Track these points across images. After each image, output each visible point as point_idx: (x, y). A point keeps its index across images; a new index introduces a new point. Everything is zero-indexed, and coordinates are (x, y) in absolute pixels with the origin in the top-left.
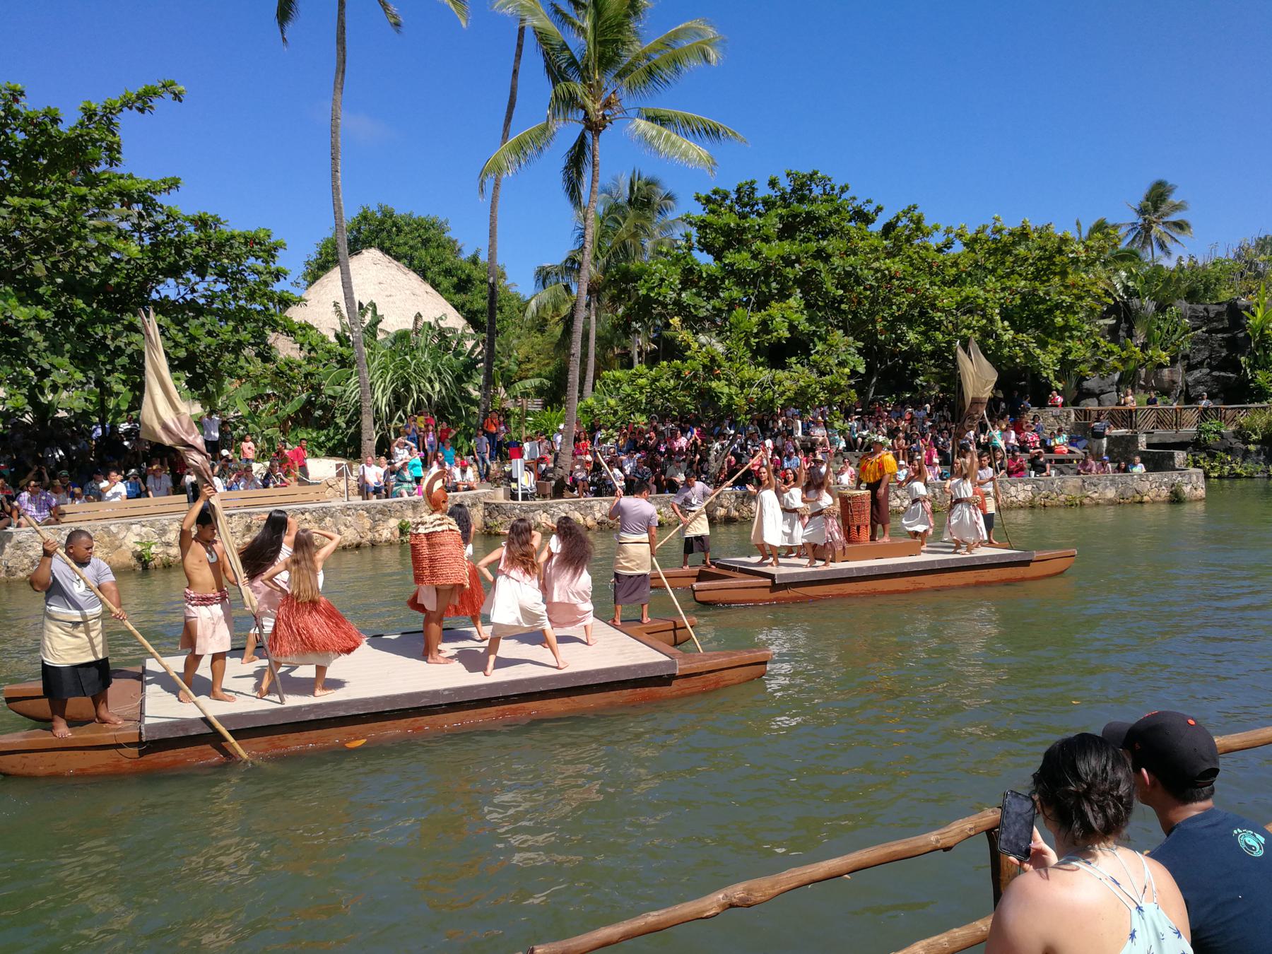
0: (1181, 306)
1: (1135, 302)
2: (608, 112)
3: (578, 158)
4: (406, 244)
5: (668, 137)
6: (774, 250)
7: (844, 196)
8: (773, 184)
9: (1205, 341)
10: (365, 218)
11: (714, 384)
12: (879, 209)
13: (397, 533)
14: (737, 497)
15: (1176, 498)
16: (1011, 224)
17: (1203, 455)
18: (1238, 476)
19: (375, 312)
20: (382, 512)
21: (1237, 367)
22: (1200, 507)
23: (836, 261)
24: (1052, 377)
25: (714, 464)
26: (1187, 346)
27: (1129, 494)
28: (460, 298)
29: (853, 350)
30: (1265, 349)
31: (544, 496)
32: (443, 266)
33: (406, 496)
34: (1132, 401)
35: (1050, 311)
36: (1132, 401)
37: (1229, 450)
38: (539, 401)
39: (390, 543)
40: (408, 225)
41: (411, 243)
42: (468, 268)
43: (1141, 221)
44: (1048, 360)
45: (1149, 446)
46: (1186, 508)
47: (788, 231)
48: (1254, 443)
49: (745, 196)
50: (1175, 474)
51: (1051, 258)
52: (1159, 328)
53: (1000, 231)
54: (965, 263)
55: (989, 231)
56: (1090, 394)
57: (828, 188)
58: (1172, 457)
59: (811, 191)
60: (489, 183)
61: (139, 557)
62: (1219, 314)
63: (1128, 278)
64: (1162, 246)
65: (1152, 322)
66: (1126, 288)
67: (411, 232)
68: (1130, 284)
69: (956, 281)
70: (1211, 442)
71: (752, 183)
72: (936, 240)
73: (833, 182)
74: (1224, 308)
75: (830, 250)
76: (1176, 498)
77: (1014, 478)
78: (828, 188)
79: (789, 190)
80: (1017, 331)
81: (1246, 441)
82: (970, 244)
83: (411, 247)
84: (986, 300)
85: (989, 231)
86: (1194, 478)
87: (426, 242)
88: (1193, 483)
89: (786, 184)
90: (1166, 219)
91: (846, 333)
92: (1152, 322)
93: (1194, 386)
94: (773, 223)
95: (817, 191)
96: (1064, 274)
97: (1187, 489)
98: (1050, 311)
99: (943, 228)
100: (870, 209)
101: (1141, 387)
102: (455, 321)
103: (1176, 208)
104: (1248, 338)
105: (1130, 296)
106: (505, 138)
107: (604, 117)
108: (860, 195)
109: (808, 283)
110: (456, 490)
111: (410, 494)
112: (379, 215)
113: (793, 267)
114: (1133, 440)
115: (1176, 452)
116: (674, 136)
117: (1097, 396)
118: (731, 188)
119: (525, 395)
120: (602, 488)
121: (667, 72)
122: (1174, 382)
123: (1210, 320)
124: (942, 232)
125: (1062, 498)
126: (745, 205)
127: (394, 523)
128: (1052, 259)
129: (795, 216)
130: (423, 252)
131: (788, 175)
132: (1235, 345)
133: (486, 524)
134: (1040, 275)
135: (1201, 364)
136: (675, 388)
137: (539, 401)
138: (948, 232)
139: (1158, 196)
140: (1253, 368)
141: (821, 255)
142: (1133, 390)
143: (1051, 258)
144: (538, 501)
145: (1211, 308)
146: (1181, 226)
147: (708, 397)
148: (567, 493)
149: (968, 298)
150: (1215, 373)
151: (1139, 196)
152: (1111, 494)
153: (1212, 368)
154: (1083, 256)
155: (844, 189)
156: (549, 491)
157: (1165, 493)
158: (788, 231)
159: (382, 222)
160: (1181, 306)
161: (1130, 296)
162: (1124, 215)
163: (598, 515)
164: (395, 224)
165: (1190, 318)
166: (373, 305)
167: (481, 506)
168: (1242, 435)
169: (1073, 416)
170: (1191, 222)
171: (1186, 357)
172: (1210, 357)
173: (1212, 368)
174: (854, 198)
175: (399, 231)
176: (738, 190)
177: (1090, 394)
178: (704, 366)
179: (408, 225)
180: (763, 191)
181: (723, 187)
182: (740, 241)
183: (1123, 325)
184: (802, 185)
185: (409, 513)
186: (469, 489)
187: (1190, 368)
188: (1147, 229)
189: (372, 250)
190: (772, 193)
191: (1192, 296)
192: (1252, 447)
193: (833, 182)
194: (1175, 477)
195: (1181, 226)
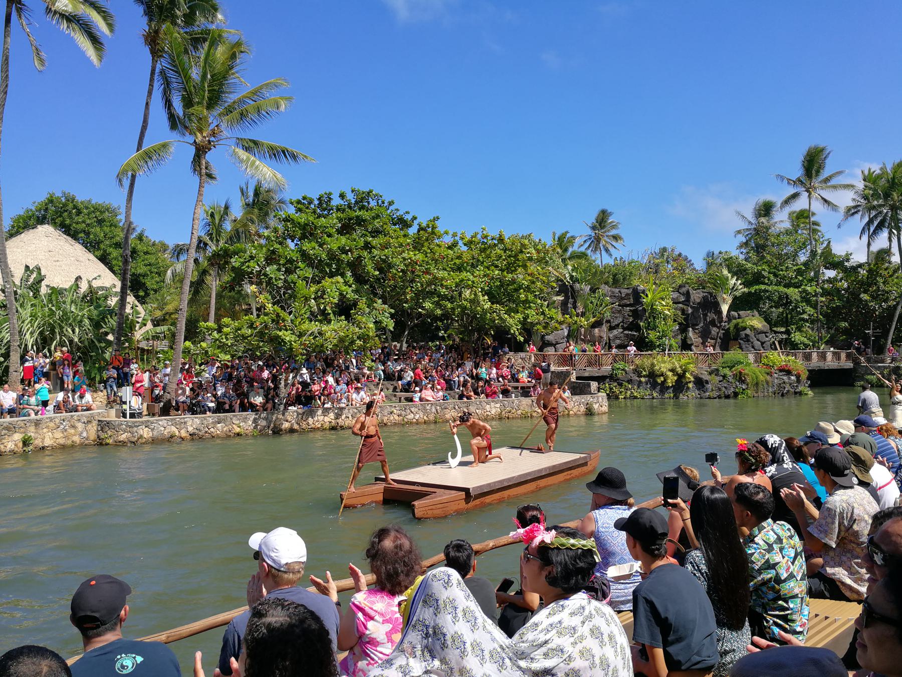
0: (604, 289)
1: (577, 286)
2: (212, 139)
4: (84, 222)
5: (254, 162)
6: (336, 243)
7: (391, 208)
8: (342, 196)
9: (620, 312)
10: (51, 201)
11: (280, 334)
12: (415, 218)
13: (21, 445)
14: (298, 414)
15: (589, 413)
16: (493, 233)
17: (615, 384)
18: (636, 398)
19: (39, 273)
20: (7, 428)
21: (638, 328)
22: (605, 418)
23: (375, 252)
24: (517, 333)
25: (283, 390)
26: (608, 315)
29: (387, 315)
30: (654, 318)
31: (154, 415)
32: (114, 241)
33: (33, 416)
34: (573, 348)
35: (516, 290)
36: (573, 348)
37: (630, 381)
39: (13, 452)
40: (87, 208)
41: (88, 221)
43: (593, 234)
44: (513, 323)
45: (578, 378)
46: (596, 418)
47: (346, 229)
48: (644, 376)
49: (324, 202)
50: (589, 396)
51: (516, 256)
52: (592, 303)
53: (486, 237)
54: (466, 257)
55: (479, 236)
56: (549, 344)
57: (380, 202)
58: (589, 385)
59: (369, 203)
60: (126, 183)
62: (627, 295)
63: (573, 270)
64: (607, 250)
65: (588, 299)
66: (572, 277)
67: (89, 214)
68: (574, 274)
69: (459, 269)
70: (619, 376)
71: (330, 194)
72: (448, 240)
73: (383, 198)
74: (630, 291)
76: (589, 413)
77: (490, 399)
78: (380, 202)
79: (353, 201)
80: (493, 303)
81: (640, 376)
82: (469, 244)
83: (88, 225)
84: (473, 282)
85: (479, 236)
86: (600, 399)
87: (100, 222)
88: (600, 402)
89: (351, 197)
90: (608, 234)
91: (384, 303)
92: (588, 299)
93: (614, 340)
94: (333, 221)
95: (373, 203)
96: (525, 267)
97: (596, 406)
98: (516, 290)
99: (451, 233)
100: (408, 217)
101: (582, 340)
102: (108, 280)
103: (614, 227)
104: (644, 310)
105: (574, 282)
107: (209, 142)
108: (403, 207)
109: (356, 265)
110: (76, 411)
111: (36, 414)
112: (63, 200)
113: (347, 254)
114: (567, 374)
115: (592, 383)
116: (258, 162)
117: (554, 345)
118: (315, 196)
120: (195, 408)
121: (253, 115)
122: (601, 337)
123: (622, 299)
124: (450, 236)
125: (519, 412)
126: (324, 210)
127: (18, 437)
128: (514, 256)
129: (350, 219)
130: (98, 229)
131: (353, 191)
132: (636, 315)
133: (98, 437)
134: (510, 268)
135: (618, 325)
136: (251, 335)
138: (454, 235)
139: (602, 220)
140: (647, 329)
141: (367, 246)
142: (576, 342)
143: (516, 256)
144: (145, 418)
145: (623, 291)
146: (616, 238)
147: (277, 342)
148: (173, 412)
149: (463, 280)
150: (626, 332)
151: (592, 219)
153: (624, 329)
154: (535, 256)
155: (391, 203)
156: (157, 410)
157: (583, 409)
158: (346, 229)
159: (65, 205)
160: (604, 289)
161: (574, 282)
162: (581, 233)
163: (190, 429)
164: (75, 207)
165: (610, 297)
166: (39, 269)
167: (95, 423)
168: (637, 372)
169: (533, 358)
170: (623, 236)
171: (608, 321)
172: (623, 322)
173: (624, 329)
174: (397, 210)
175: (79, 212)
176: (319, 199)
177: (549, 344)
178: (273, 321)
179: (87, 208)
180: (336, 201)
181: (309, 195)
182: (311, 234)
183: (571, 300)
184: (362, 199)
185: (32, 429)
187: (611, 328)
188: (598, 240)
189: (46, 226)
190: (342, 202)
191: (616, 282)
192: (643, 379)
193: (383, 198)
194: (588, 398)
195: (616, 238)
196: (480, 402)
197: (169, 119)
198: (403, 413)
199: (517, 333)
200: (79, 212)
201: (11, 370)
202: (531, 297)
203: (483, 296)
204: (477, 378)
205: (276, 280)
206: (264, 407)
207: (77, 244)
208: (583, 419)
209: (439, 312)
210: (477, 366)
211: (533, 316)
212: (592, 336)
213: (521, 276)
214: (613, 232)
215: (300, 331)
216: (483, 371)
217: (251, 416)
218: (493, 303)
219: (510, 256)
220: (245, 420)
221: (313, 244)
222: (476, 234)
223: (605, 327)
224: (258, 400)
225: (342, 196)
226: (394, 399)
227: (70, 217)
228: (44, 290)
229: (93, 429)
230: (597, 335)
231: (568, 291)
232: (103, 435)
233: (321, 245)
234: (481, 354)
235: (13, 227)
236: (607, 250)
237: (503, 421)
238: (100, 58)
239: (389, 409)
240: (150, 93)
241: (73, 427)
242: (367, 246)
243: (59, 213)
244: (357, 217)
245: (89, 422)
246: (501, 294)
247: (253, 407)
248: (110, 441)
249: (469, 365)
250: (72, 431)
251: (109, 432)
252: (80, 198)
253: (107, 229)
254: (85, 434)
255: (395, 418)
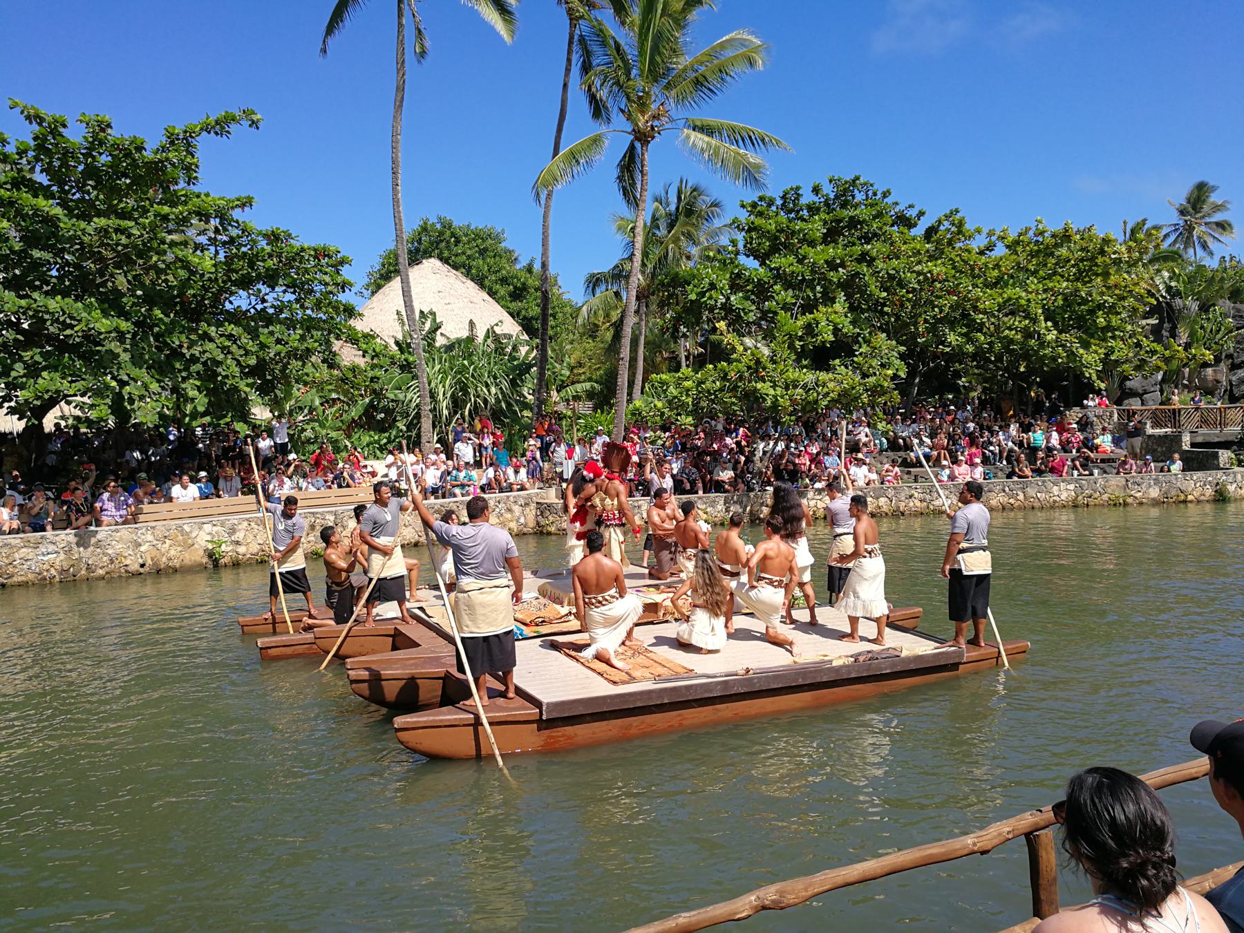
1: (1178, 302)
3: (629, 166)
4: (464, 253)
6: (819, 255)
8: (816, 190)
10: (424, 229)
12: (921, 214)
16: (1055, 227)
19: (434, 320)
23: (880, 264)
24: (1094, 377)
27: (1173, 493)
28: (515, 305)
34: (1178, 399)
35: (1092, 312)
38: (590, 404)
41: (469, 252)
42: (523, 276)
43: (1182, 223)
44: (1091, 359)
45: (1193, 445)
46: (1231, 508)
47: (831, 236)
50: (1220, 473)
51: (1093, 259)
52: (1202, 327)
53: (1042, 233)
54: (1007, 266)
55: (1031, 233)
56: (1133, 394)
57: (870, 193)
58: (1216, 456)
59: (853, 197)
61: (211, 555)
63: (1171, 278)
64: (1204, 246)
66: (1169, 289)
67: (469, 242)
68: (1173, 284)
71: (798, 188)
72: (979, 242)
73: (875, 187)
75: (874, 253)
78: (870, 193)
79: (832, 196)
80: (1060, 332)
82: (1013, 246)
83: (469, 257)
84: (1029, 301)
85: (1031, 233)
89: (829, 190)
90: (1207, 220)
94: (817, 227)
95: (859, 197)
97: (1231, 488)
98: (1092, 312)
99: (985, 231)
100: (912, 213)
102: (510, 327)
103: (1217, 208)
105: (1173, 297)
106: (556, 152)
108: (902, 199)
109: (851, 286)
112: (438, 226)
114: (1175, 440)
115: (1221, 452)
117: (1140, 396)
119: (577, 398)
122: (1218, 382)
124: (984, 235)
125: (1105, 497)
128: (1094, 259)
129: (840, 221)
133: (538, 523)
137: (590, 404)
138: (990, 234)
139: (1198, 198)
141: (864, 258)
143: (1093, 259)
146: (1223, 226)
151: (1181, 196)
152: (1154, 493)
155: (886, 194)
157: (1209, 492)
158: (831, 236)
159: (441, 233)
161: (1173, 297)
162: (1165, 216)
164: (453, 235)
165: (1233, 317)
167: (533, 506)
169: (1116, 416)
171: (1230, 356)
174: (897, 204)
175: (458, 242)
176: (784, 197)
177: (1133, 394)
179: (466, 235)
180: (807, 198)
184: (845, 190)
186: (523, 488)
189: (432, 260)
190: (816, 199)
193: (875, 187)
195: (1223, 226)
196: (1044, 482)
197: (591, 103)
198: (928, 497)
199: (1094, 377)
200: (458, 242)
201: (424, 440)
202: (1115, 321)
203: (1046, 321)
204: (1032, 450)
205: (746, 314)
206: (734, 483)
207: (469, 281)
208: (1208, 508)
209: (970, 348)
210: (1026, 428)
211: (1121, 350)
212: (1203, 380)
213: (1095, 290)
214: (1218, 217)
215: (788, 383)
216: (1038, 437)
217: (720, 498)
218: (1060, 332)
219: (1082, 260)
220: (713, 504)
221: (792, 259)
222: (1027, 230)
223: (1223, 367)
224: (726, 475)
225: (816, 190)
226: (906, 477)
227: (448, 247)
228: (440, 341)
229: (531, 512)
230: (1210, 378)
231: (1166, 315)
232: (543, 522)
233: (800, 261)
234: (1030, 412)
235: (383, 265)
236: (1204, 246)
237: (1080, 510)
238: (512, 32)
239: (907, 492)
240: (568, 70)
241: (510, 510)
242: (864, 258)
243: (435, 244)
244: (851, 218)
245: (527, 504)
246: (1076, 317)
247: (718, 487)
248: (552, 529)
249: (1013, 429)
250: (509, 516)
251: (551, 518)
252: (458, 223)
253: (490, 261)
254: (522, 520)
255: (915, 504)
